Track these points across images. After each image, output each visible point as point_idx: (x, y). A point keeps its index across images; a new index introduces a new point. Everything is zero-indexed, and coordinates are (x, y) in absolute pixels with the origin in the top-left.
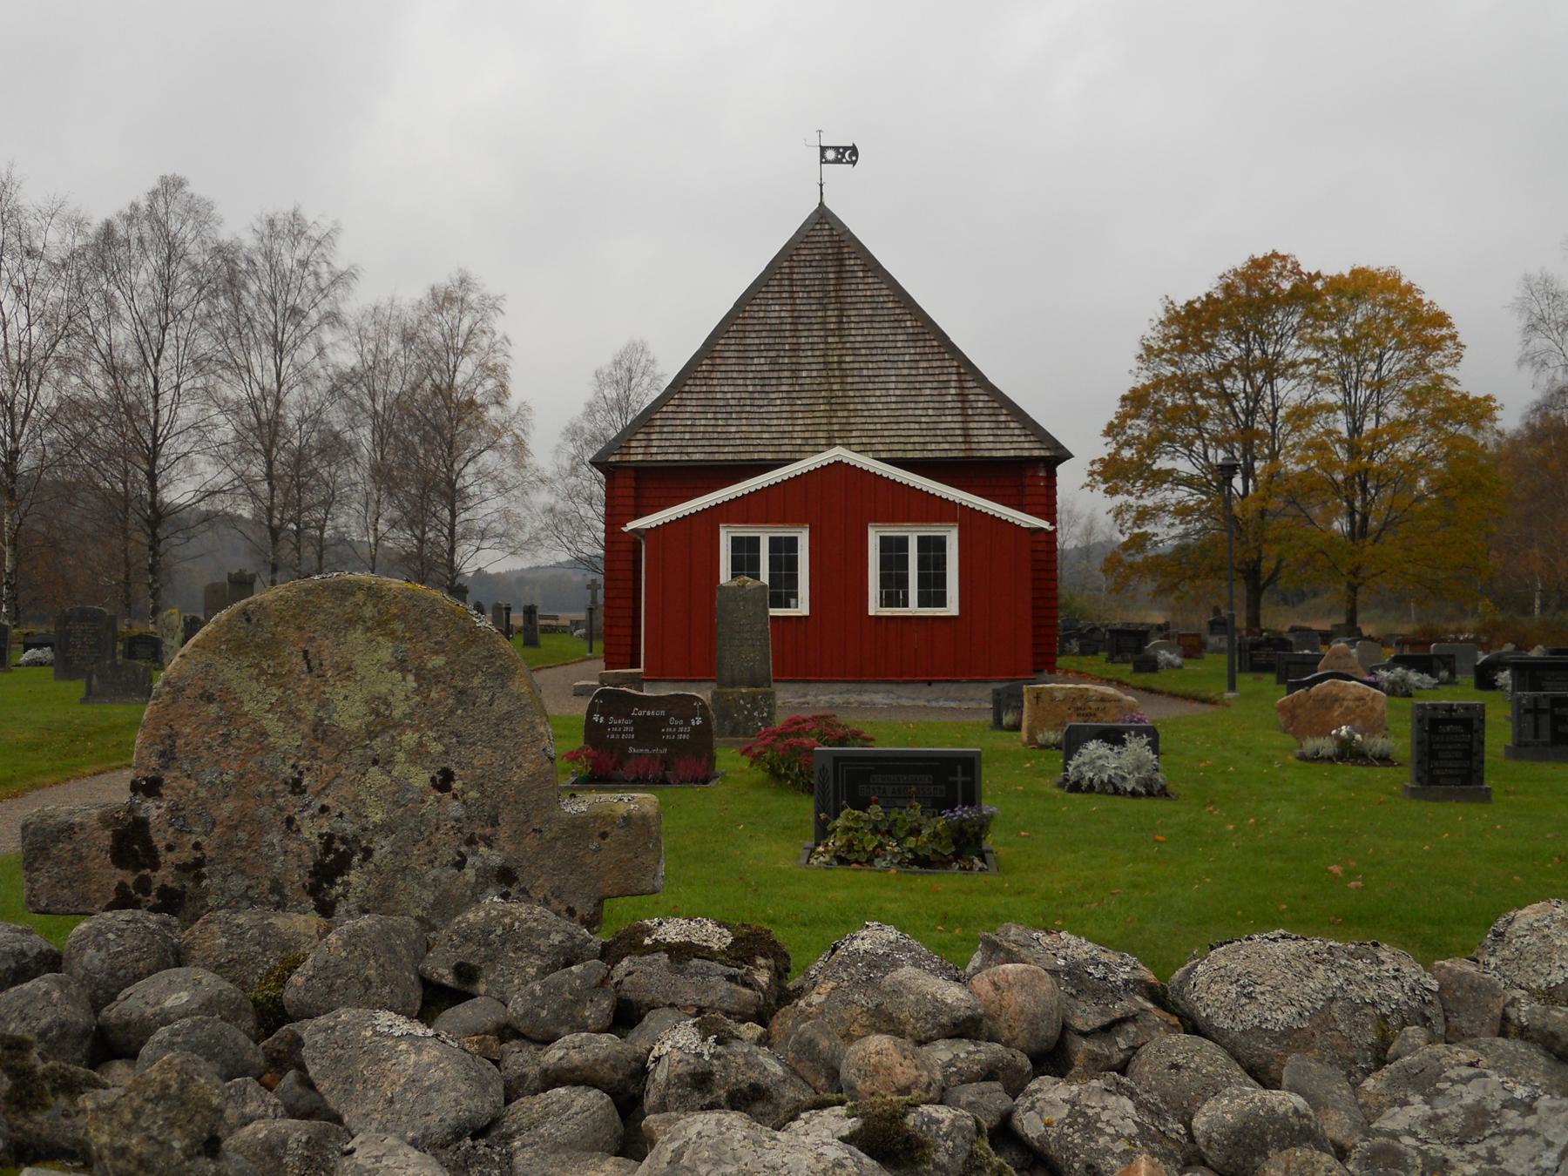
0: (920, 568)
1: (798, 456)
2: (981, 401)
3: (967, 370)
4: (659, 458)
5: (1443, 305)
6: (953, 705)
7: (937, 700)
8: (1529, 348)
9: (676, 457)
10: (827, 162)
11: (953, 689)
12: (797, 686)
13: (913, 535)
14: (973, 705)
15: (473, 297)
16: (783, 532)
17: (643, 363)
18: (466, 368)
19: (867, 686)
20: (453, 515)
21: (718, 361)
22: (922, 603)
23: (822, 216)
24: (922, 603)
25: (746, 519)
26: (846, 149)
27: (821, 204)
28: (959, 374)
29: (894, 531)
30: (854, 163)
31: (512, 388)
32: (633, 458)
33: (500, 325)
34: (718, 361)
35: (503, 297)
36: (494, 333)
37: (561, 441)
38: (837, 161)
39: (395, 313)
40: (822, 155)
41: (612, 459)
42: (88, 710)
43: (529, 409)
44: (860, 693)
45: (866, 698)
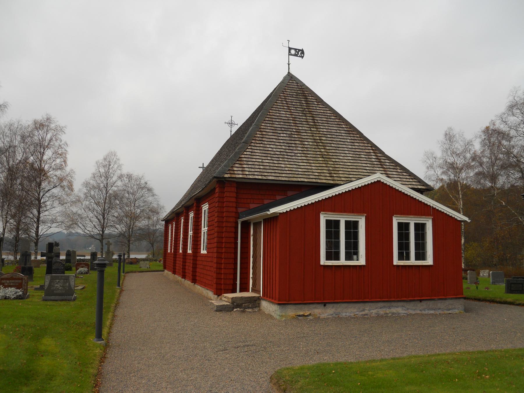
1: (370, 174)
3: (376, 149)
4: (251, 177)
6: (432, 312)
7: (424, 310)
8: (428, 174)
9: (260, 177)
10: (291, 55)
11: (431, 303)
13: (412, 221)
14: (440, 312)
15: (52, 126)
16: (352, 218)
17: (115, 160)
18: (48, 154)
20: (39, 213)
21: (264, 133)
22: (417, 259)
23: (290, 78)
24: (417, 259)
25: (333, 210)
26: (299, 50)
27: (289, 73)
28: (373, 150)
29: (404, 220)
30: (302, 57)
31: (68, 162)
32: (237, 176)
33: (64, 138)
34: (264, 133)
35: (65, 127)
36: (61, 141)
37: (81, 187)
38: (295, 55)
39: (20, 127)
40: (289, 52)
41: (226, 176)
43: (74, 172)
44: (389, 308)
45: (394, 310)
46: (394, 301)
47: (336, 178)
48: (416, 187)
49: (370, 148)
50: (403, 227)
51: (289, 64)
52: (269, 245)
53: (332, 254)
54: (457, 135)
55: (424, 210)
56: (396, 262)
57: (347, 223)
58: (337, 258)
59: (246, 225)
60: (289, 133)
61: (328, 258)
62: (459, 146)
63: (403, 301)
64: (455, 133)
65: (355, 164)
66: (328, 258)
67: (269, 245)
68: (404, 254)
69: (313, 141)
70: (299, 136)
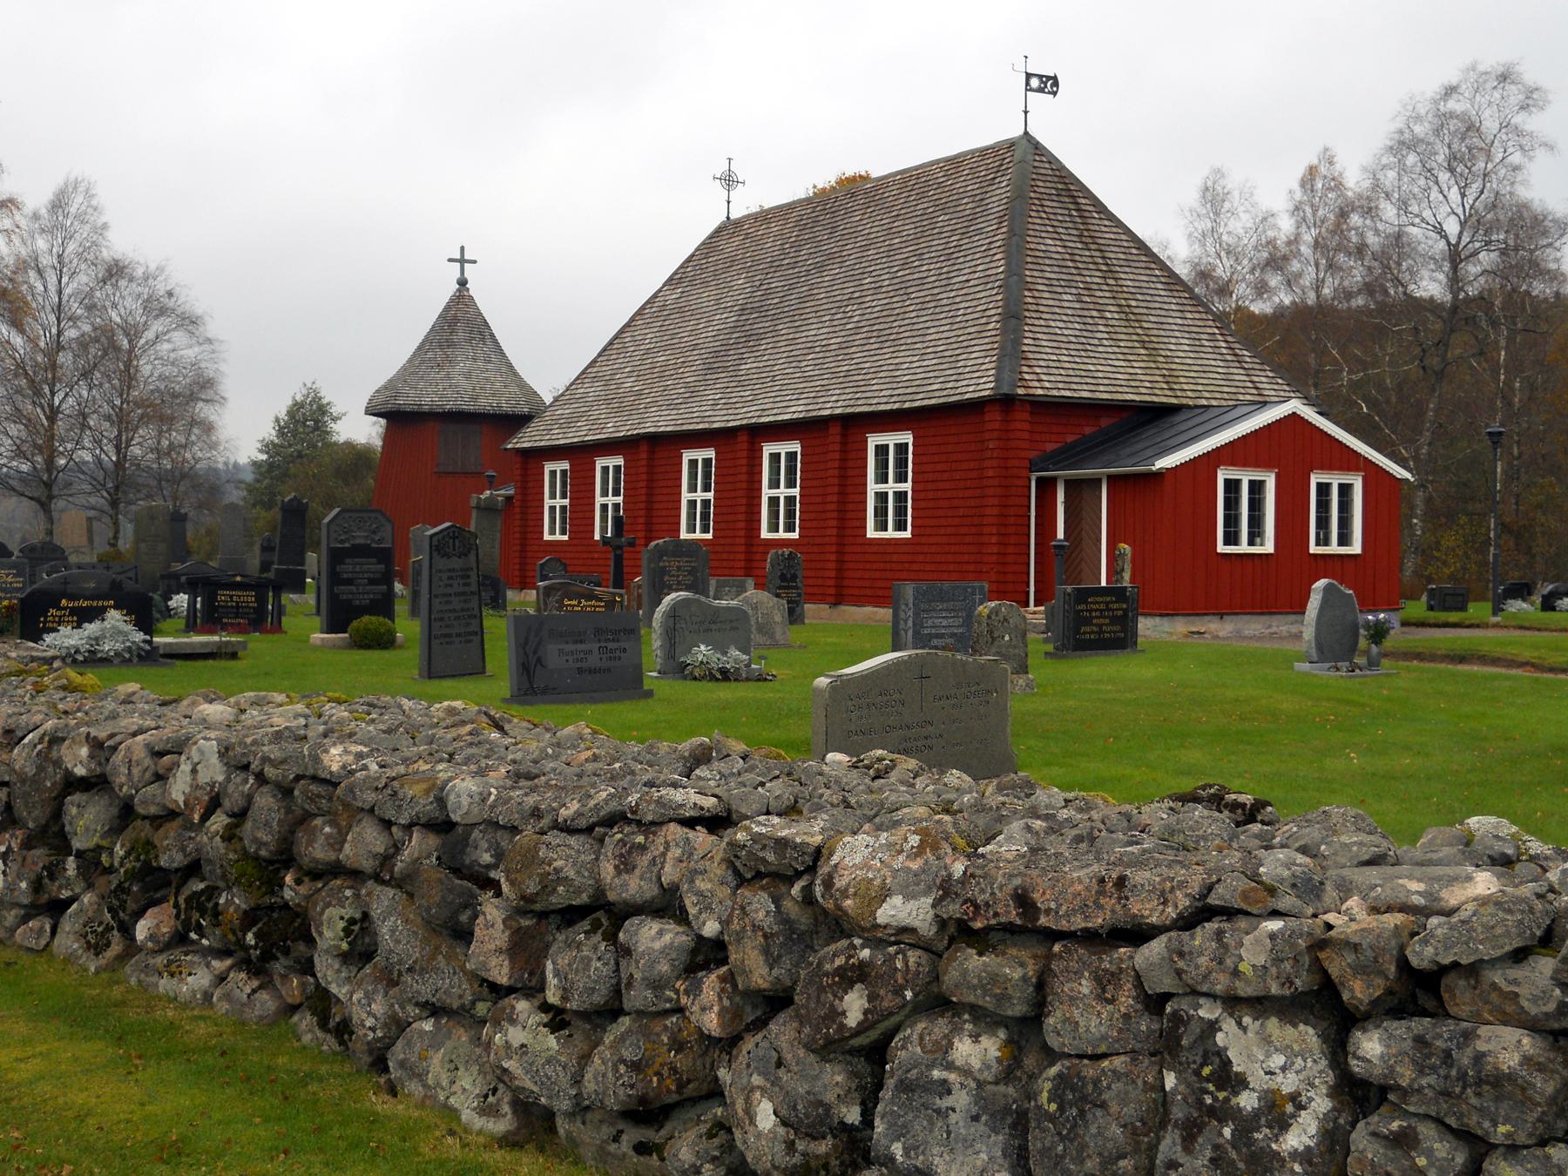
0: (876, 515)
4: (1055, 393)
5: (198, 309)
9: (1068, 394)
13: (1335, 480)
16: (1257, 476)
26: (1049, 78)
27: (1026, 133)
29: (1324, 478)
30: (1055, 94)
38: (1041, 90)
40: (1027, 83)
41: (1020, 391)
42: (1432, 614)
45: (1536, 654)
50: (1324, 489)
51: (1026, 112)
53: (1232, 538)
54: (1236, 194)
55: (1351, 461)
56: (1313, 549)
57: (1251, 483)
59: (1047, 486)
61: (1227, 543)
62: (1238, 227)
64: (1229, 186)
66: (1227, 543)
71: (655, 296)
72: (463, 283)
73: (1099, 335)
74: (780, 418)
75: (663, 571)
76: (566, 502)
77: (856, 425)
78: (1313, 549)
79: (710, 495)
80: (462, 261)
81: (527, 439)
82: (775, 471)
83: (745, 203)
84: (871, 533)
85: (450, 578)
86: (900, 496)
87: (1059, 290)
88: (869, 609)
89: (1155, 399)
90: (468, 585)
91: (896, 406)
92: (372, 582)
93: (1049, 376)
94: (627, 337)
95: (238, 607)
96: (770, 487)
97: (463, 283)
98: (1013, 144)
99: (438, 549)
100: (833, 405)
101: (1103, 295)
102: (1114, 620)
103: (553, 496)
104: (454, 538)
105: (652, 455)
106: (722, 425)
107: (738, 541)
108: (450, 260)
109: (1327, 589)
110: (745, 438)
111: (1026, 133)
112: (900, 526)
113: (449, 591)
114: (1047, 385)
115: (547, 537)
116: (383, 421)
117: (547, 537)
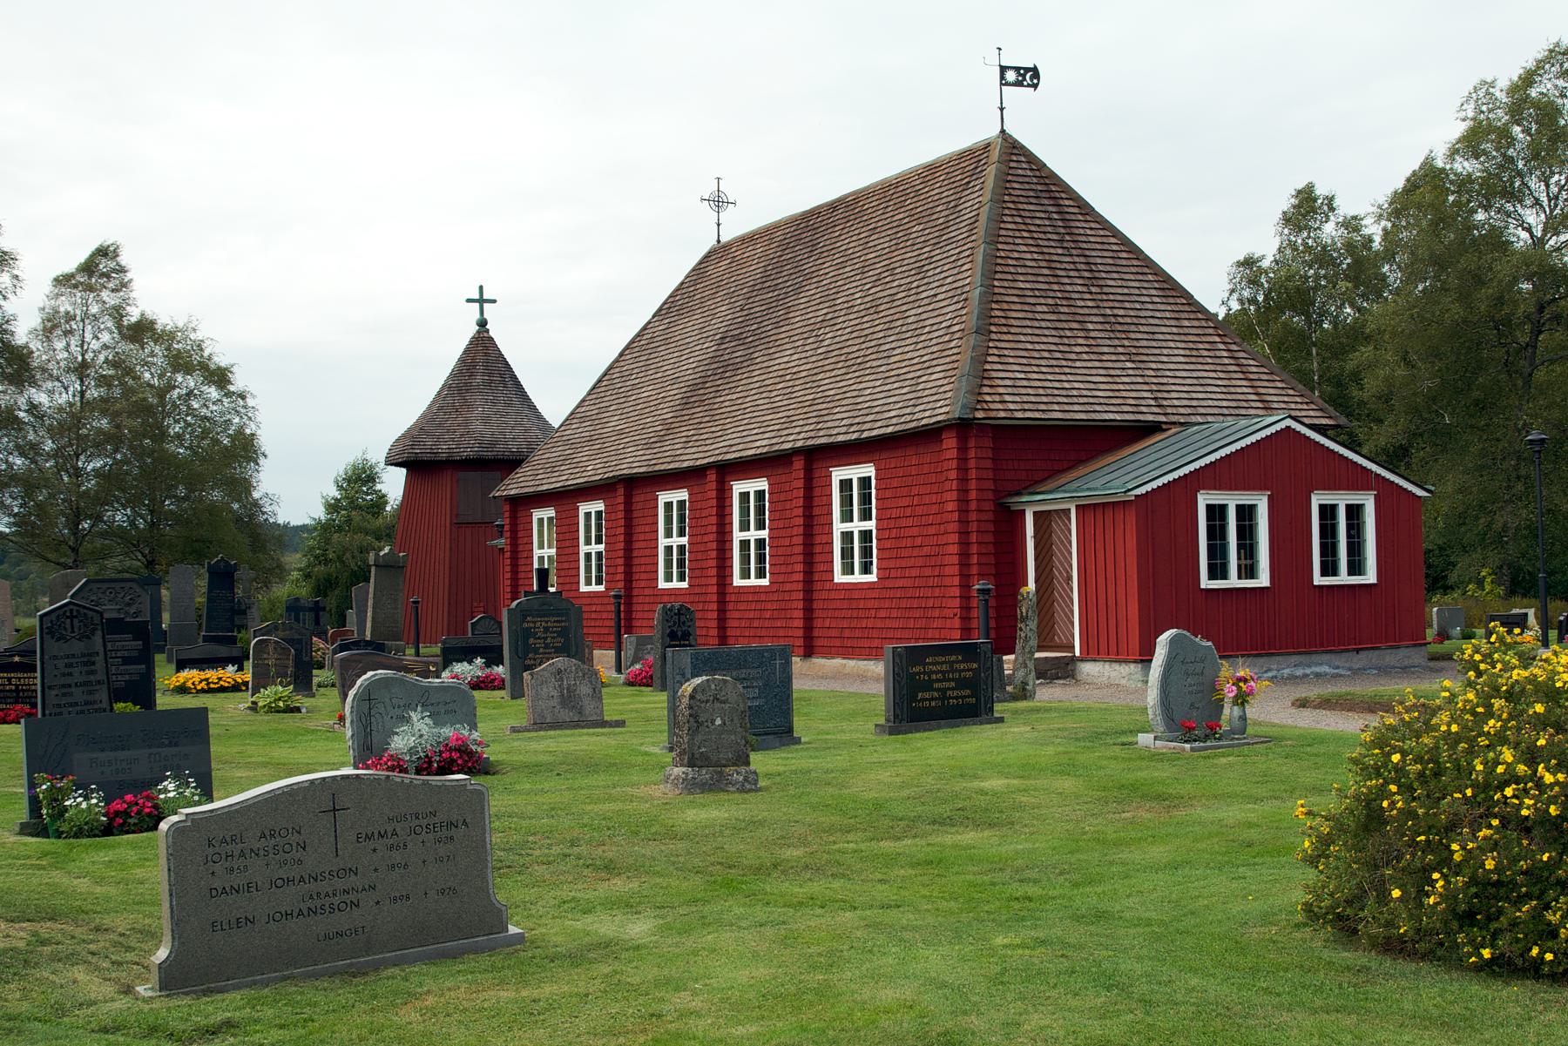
2: (1023, 170)
10: (1007, 84)
12: (1262, 660)
13: (1341, 500)
16: (1246, 498)
19: (1315, 658)
23: (1012, 149)
26: (1027, 70)
27: (1003, 131)
30: (1035, 86)
38: (1018, 84)
40: (1002, 77)
41: (980, 415)
46: (1316, 652)
47: (1169, 410)
48: (1316, 421)
49: (1211, 331)
50: (1328, 512)
51: (1002, 109)
52: (1101, 555)
53: (1218, 571)
56: (1318, 580)
57: (1240, 508)
58: (1225, 576)
60: (1050, 301)
61: (1212, 576)
63: (1331, 652)
65: (1195, 374)
66: (1212, 576)
67: (1101, 555)
68: (1329, 568)
69: (1100, 319)
70: (1073, 310)
71: (645, 328)
72: (483, 323)
73: (1078, 349)
74: (728, 457)
75: (527, 633)
76: (684, 540)
77: (820, 456)
78: (1318, 580)
79: (871, 525)
80: (481, 301)
81: (517, 484)
82: (847, 501)
83: (736, 225)
84: (839, 578)
85: (71, 665)
86: (866, 536)
87: (1032, 301)
88: (838, 662)
89: (1141, 417)
90: (93, 672)
91: (855, 436)
92: (127, 661)
93: (1022, 395)
94: (616, 373)
95: (17, 691)
96: (843, 521)
97: (483, 323)
98: (989, 145)
99: (51, 632)
100: (794, 439)
101: (1085, 304)
102: (961, 684)
103: (669, 534)
104: (72, 617)
105: (629, 493)
106: (691, 463)
107: (948, 571)
108: (469, 301)
109: (1173, 642)
110: (714, 477)
111: (1003, 131)
112: (866, 569)
113: (69, 680)
114: (1012, 406)
115: (662, 584)
116: (404, 471)
117: (662, 584)
